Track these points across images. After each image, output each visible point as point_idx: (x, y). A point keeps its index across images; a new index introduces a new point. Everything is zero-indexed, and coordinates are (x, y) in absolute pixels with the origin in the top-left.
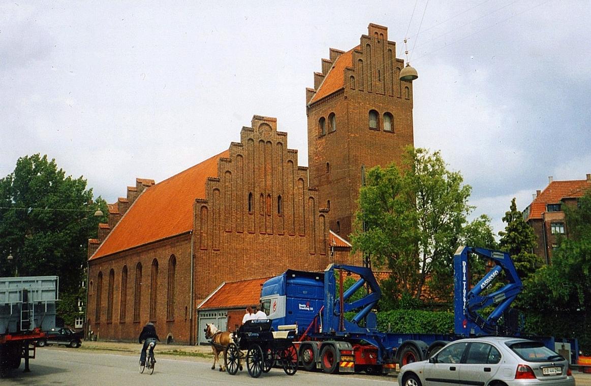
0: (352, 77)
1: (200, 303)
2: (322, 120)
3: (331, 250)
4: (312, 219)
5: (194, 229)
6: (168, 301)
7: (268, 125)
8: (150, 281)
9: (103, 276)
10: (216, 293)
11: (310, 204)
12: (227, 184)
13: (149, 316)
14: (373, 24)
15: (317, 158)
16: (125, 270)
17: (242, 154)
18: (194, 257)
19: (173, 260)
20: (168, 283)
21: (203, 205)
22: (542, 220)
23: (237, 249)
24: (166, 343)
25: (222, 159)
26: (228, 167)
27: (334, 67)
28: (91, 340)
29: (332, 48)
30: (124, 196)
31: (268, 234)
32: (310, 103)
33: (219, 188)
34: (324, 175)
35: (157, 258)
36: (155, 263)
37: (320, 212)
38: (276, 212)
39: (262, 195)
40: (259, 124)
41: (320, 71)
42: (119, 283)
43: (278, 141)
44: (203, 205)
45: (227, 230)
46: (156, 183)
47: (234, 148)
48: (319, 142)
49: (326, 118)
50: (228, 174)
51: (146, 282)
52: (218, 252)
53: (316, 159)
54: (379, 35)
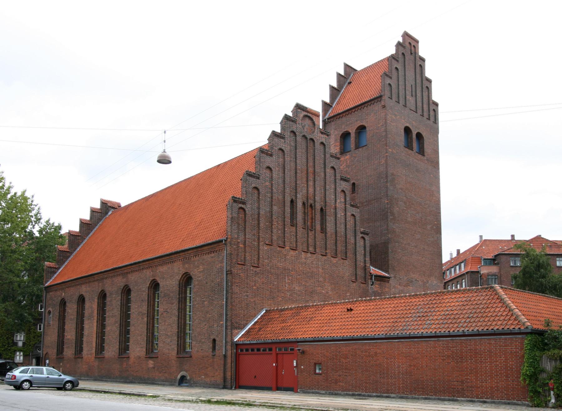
1: (238, 334)
3: (371, 279)
5: (229, 237)
6: (178, 332)
9: (67, 304)
13: (145, 350)
16: (103, 296)
18: (229, 273)
19: (187, 280)
20: (179, 309)
22: (478, 272)
23: (278, 268)
24: (177, 384)
26: (268, 161)
30: (76, 228)
32: (327, 117)
33: (259, 187)
36: (155, 286)
37: (362, 233)
38: (318, 227)
39: (304, 204)
40: (302, 115)
42: (93, 312)
43: (321, 141)
44: (240, 205)
45: (267, 243)
46: (123, 205)
47: (276, 140)
49: (353, 132)
52: (258, 269)
54: (412, 46)
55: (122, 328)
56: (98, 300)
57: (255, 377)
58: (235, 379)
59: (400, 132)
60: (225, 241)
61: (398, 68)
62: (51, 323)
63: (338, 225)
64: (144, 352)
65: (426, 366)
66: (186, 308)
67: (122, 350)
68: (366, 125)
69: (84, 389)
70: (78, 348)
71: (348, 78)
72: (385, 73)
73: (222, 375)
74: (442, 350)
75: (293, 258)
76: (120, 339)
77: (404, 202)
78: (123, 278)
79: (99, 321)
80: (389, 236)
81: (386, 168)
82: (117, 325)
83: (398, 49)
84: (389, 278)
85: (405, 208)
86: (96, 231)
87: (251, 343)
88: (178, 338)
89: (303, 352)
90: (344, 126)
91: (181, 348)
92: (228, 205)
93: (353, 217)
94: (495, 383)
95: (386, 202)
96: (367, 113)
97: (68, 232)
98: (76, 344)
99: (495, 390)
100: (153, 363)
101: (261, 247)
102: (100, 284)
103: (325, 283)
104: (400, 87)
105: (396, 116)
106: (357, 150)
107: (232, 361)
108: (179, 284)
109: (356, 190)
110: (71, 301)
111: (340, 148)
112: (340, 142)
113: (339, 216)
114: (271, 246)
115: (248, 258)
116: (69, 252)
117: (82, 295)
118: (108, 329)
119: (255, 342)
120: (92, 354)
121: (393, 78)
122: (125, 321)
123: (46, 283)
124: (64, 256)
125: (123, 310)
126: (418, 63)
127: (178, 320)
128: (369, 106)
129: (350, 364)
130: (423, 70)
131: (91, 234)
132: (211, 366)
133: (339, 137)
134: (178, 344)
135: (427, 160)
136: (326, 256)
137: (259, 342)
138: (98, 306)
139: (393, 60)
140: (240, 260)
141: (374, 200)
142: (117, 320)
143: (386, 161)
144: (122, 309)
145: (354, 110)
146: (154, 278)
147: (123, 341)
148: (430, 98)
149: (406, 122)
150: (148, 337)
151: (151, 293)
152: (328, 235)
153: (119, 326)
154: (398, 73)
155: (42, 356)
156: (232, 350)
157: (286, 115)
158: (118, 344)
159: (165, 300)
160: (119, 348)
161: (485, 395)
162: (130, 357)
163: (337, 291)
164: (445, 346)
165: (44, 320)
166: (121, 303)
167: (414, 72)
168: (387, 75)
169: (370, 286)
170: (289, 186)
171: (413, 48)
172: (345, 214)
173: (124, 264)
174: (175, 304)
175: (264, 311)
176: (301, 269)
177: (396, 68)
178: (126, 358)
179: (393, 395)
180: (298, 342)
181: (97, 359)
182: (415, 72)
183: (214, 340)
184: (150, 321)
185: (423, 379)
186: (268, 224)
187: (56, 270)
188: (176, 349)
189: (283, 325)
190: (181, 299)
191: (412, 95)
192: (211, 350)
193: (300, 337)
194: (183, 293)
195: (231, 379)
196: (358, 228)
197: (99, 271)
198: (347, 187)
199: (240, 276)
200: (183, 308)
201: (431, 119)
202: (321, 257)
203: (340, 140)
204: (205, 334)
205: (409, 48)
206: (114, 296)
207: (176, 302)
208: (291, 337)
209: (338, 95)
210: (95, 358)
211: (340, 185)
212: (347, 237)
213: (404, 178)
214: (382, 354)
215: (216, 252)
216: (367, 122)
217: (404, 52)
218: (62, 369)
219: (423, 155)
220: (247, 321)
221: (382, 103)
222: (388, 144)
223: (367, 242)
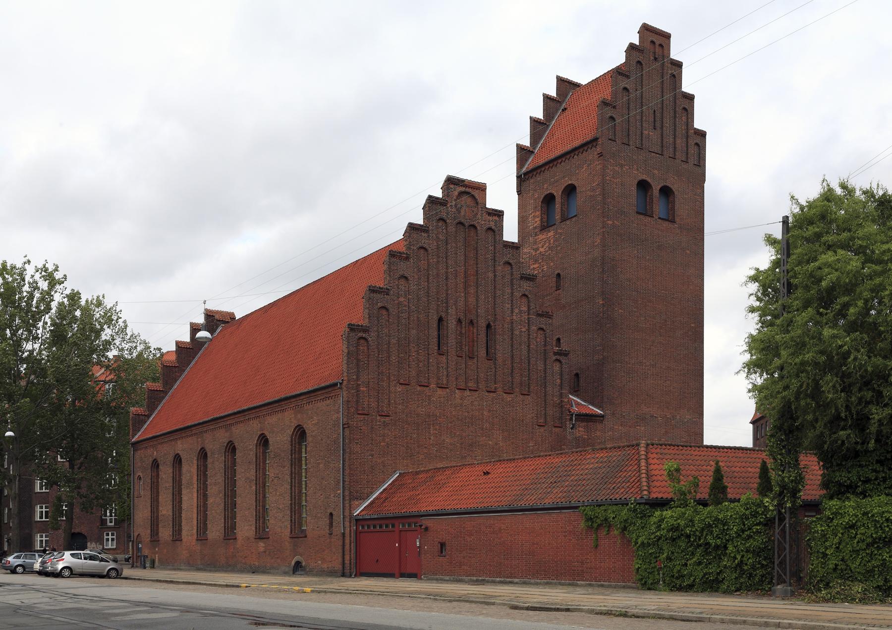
0: (612, 118)
1: (359, 506)
2: (549, 199)
3: (571, 419)
4: (541, 366)
6: (291, 504)
7: (473, 197)
8: (253, 472)
9: (161, 467)
10: (385, 490)
11: (538, 340)
12: (402, 299)
13: (254, 529)
16: (203, 455)
17: (425, 246)
19: (300, 434)
20: (291, 474)
21: (360, 334)
23: (418, 415)
24: (291, 572)
25: (392, 254)
26: (403, 268)
28: (145, 568)
29: (561, 75)
31: (470, 390)
32: (524, 170)
33: (389, 306)
35: (267, 433)
36: (264, 441)
37: (555, 354)
38: (483, 353)
39: (459, 321)
40: (456, 193)
41: (539, 115)
43: (487, 226)
44: (360, 334)
45: (402, 381)
46: (238, 316)
47: (415, 235)
48: (541, 237)
49: (558, 194)
50: (402, 282)
51: (245, 474)
52: (387, 419)
53: (534, 268)
54: (657, 46)
55: (228, 499)
56: (198, 461)
57: (377, 561)
58: (355, 565)
60: (341, 384)
62: (142, 493)
64: (253, 531)
65: (549, 544)
66: (302, 472)
67: (228, 530)
68: (576, 185)
69: (597, 614)
70: (176, 527)
71: (564, 101)
72: (603, 102)
73: (340, 559)
74: (564, 524)
75: (442, 400)
76: (225, 515)
78: (226, 431)
79: (200, 490)
82: (221, 495)
84: (603, 416)
86: (200, 357)
87: (372, 517)
88: (291, 512)
89: (426, 529)
91: (295, 525)
92: (344, 336)
94: (613, 563)
95: (601, 303)
98: (173, 521)
99: (613, 571)
100: (264, 545)
101: (392, 389)
102: (199, 440)
103: (493, 431)
105: (622, 166)
107: (350, 541)
108: (292, 441)
110: (164, 463)
114: (407, 386)
115: (373, 404)
116: (162, 391)
117: (178, 454)
118: (210, 501)
119: (375, 517)
120: (193, 535)
122: (231, 490)
123: (133, 437)
124: (155, 398)
125: (228, 475)
127: (291, 488)
129: (474, 543)
131: (193, 363)
132: (328, 549)
134: (291, 520)
136: (495, 392)
137: (379, 516)
138: (198, 469)
140: (361, 409)
142: (220, 489)
144: (227, 474)
145: (560, 161)
146: (262, 432)
147: (230, 516)
148: (689, 126)
150: (258, 511)
151: (260, 452)
152: (500, 361)
153: (223, 497)
155: (133, 539)
156: (350, 528)
157: (430, 197)
158: (223, 520)
159: (276, 462)
160: (225, 527)
161: (603, 577)
162: (237, 538)
163: (512, 441)
164: (567, 520)
165: (133, 489)
166: (225, 465)
169: (569, 430)
170: (436, 299)
171: (658, 49)
172: (528, 330)
173: (226, 413)
174: (286, 468)
175: (398, 474)
176: (454, 413)
178: (232, 540)
179: (516, 580)
180: (422, 516)
181: (200, 542)
183: (331, 514)
184: (259, 490)
185: (545, 559)
186: (403, 355)
187: (146, 418)
188: (289, 526)
189: (412, 493)
190: (293, 460)
191: (654, 126)
192: (328, 527)
193: (424, 508)
194: (297, 453)
195: (350, 564)
197: (196, 422)
198: (531, 289)
199: (361, 429)
200: (297, 472)
202: (487, 394)
204: (321, 507)
206: (216, 456)
207: (287, 464)
208: (414, 510)
210: (197, 540)
214: (506, 530)
215: (332, 399)
216: (578, 179)
218: (158, 556)
219: (673, 221)
220: (372, 488)
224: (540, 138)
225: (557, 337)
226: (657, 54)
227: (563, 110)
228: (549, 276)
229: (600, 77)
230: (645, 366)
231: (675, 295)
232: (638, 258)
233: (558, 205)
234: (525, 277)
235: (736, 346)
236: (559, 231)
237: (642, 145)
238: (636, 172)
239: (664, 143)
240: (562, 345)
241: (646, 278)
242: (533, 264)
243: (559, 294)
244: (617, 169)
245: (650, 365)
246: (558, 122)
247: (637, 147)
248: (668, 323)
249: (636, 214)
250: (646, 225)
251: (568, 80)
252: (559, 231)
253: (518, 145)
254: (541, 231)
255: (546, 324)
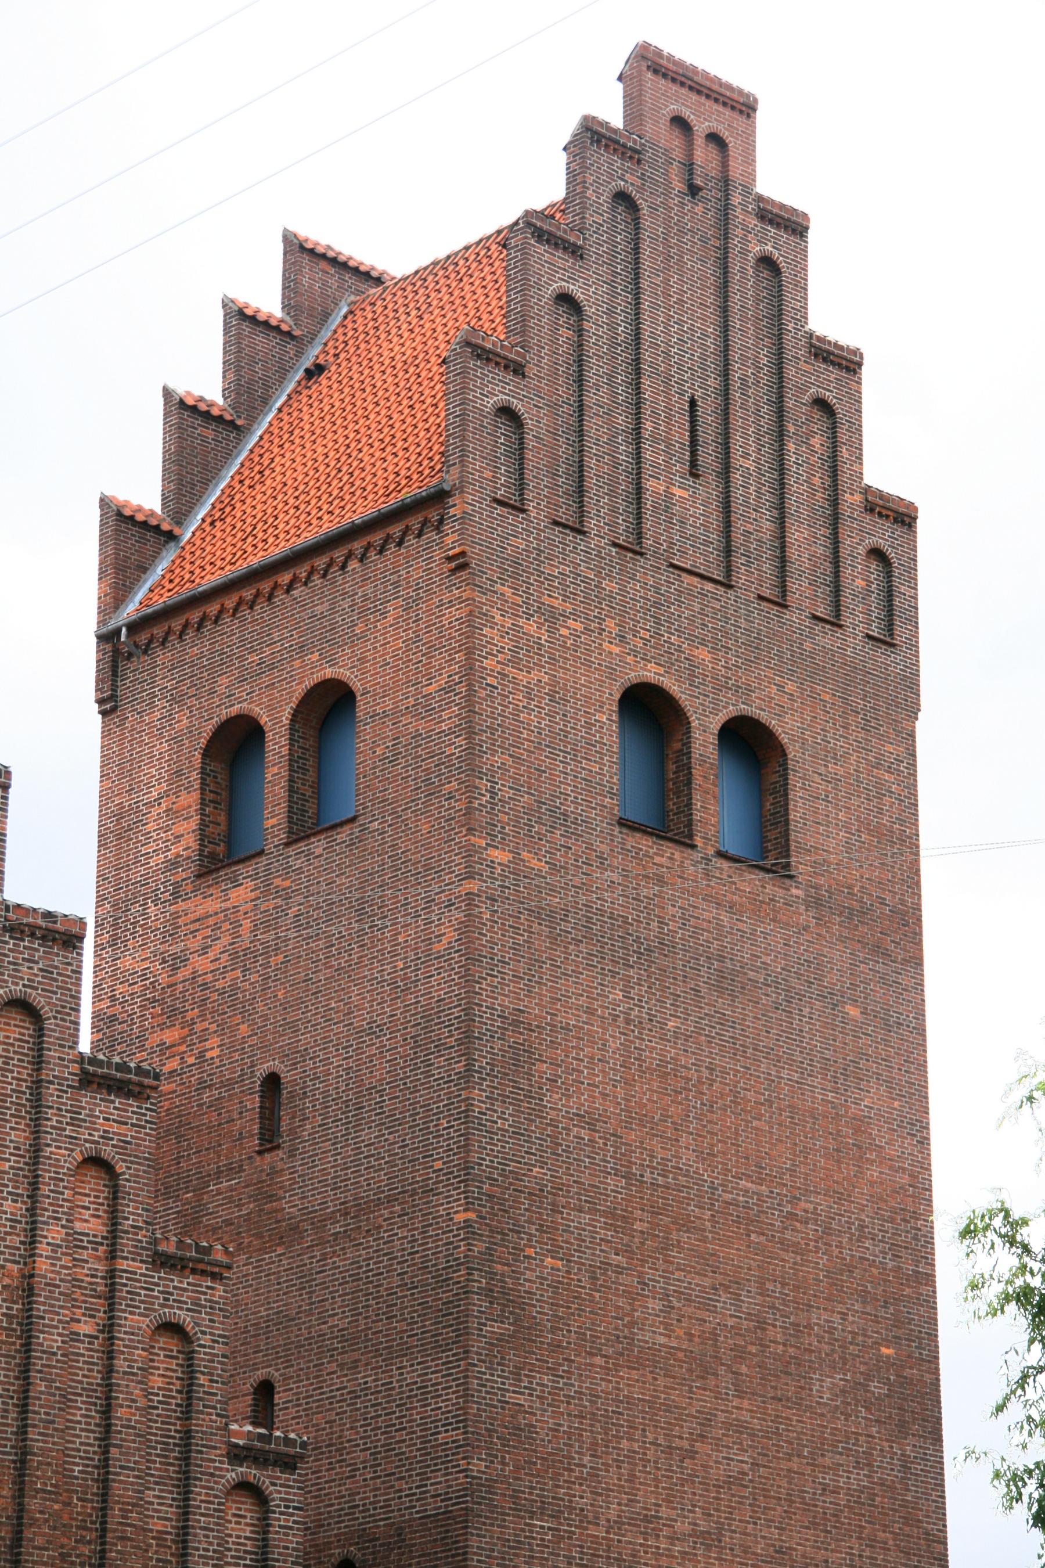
14: (659, 53)
15: (170, 1036)
27: (315, 371)
32: (131, 610)
34: (233, 1170)
37: (237, 1455)
53: (164, 1048)
54: (699, 141)
59: (589, 725)
61: (579, 295)
63: (39, 1410)
68: (357, 686)
71: (313, 336)
72: (468, 344)
77: (611, 1214)
80: (478, 1465)
81: (468, 980)
83: (584, 168)
85: (615, 1259)
90: (224, 680)
93: (174, 1345)
95: (460, 1218)
96: (365, 598)
97: (100, 716)
104: (593, 425)
105: (552, 618)
106: (302, 846)
109: (284, 1126)
111: (203, 825)
112: (203, 784)
113: (50, 1340)
121: (531, 370)
126: (744, 252)
128: (372, 555)
130: (788, 288)
133: (198, 755)
135: (815, 902)
139: (541, 248)
141: (391, 1200)
143: (468, 928)
145: (285, 578)
148: (844, 478)
149: (634, 652)
154: (580, 332)
167: (712, 314)
168: (484, 355)
171: (704, 155)
172: (109, 1328)
177: (565, 299)
182: (725, 310)
191: (693, 463)
196: (206, 1421)
201: (847, 620)
203: (203, 772)
205: (678, 154)
209: (228, 456)
211: (75, 1122)
212: (117, 1490)
213: (613, 1044)
216: (363, 660)
217: (629, 183)
219: (782, 871)
221: (449, 540)
222: (482, 818)
223: (279, 1520)
224: (206, 483)
225: (261, 1374)
226: (698, 171)
227: (310, 374)
228: (229, 1084)
229: (467, 248)
230: (672, 1539)
231: (803, 1205)
232: (628, 1021)
233: (275, 770)
234: (104, 1077)
235: (1029, 1350)
236: (277, 882)
237: (640, 536)
238: (616, 650)
239: (738, 538)
240: (280, 1415)
241: (665, 1117)
242: (162, 1027)
243: (274, 1172)
244: (532, 628)
245: (694, 1534)
246: (286, 418)
247: (615, 545)
248: (771, 1332)
249: (617, 829)
250: (661, 881)
251: (331, 254)
252: (277, 882)
253: (105, 503)
254: (199, 876)
255: (196, 1307)
